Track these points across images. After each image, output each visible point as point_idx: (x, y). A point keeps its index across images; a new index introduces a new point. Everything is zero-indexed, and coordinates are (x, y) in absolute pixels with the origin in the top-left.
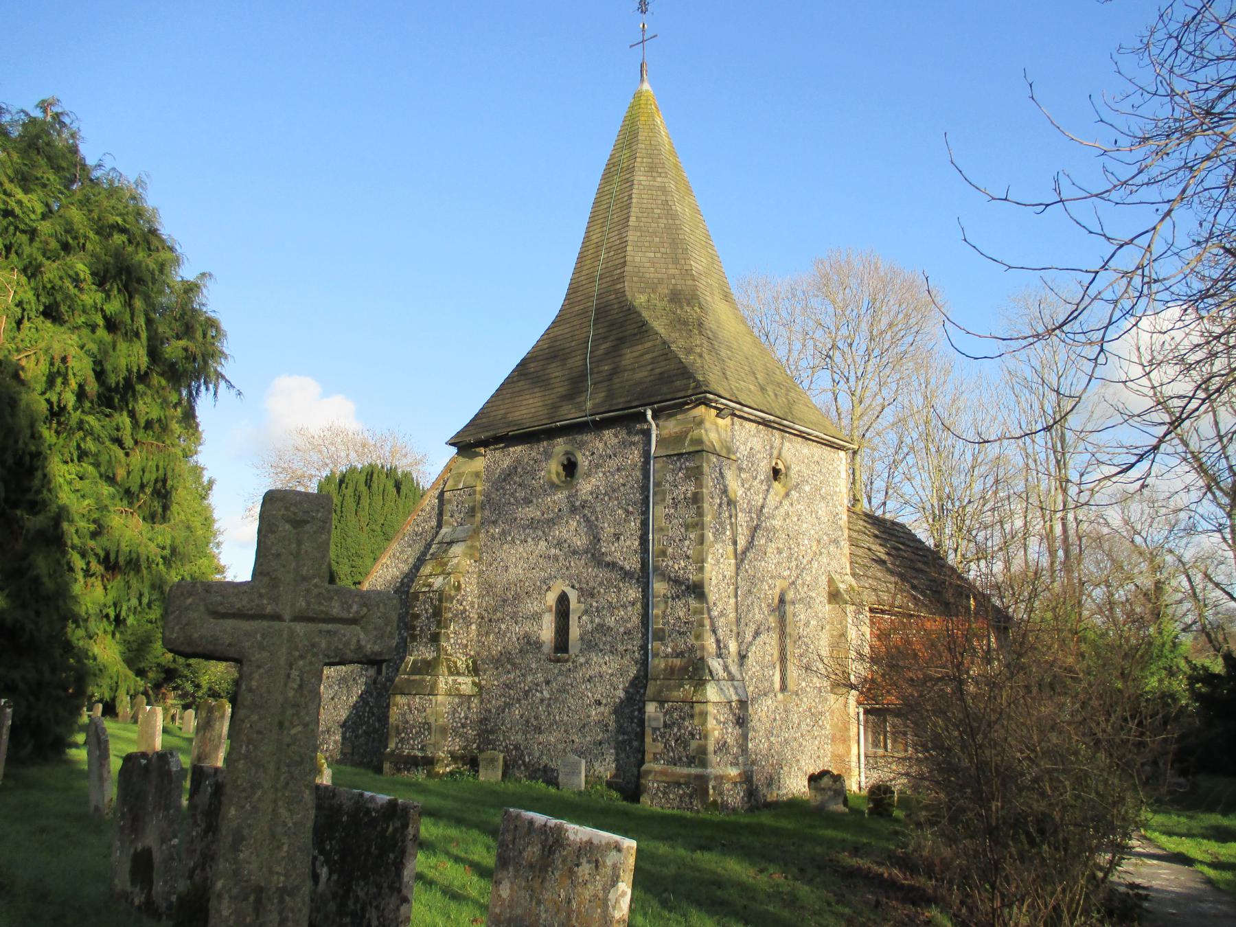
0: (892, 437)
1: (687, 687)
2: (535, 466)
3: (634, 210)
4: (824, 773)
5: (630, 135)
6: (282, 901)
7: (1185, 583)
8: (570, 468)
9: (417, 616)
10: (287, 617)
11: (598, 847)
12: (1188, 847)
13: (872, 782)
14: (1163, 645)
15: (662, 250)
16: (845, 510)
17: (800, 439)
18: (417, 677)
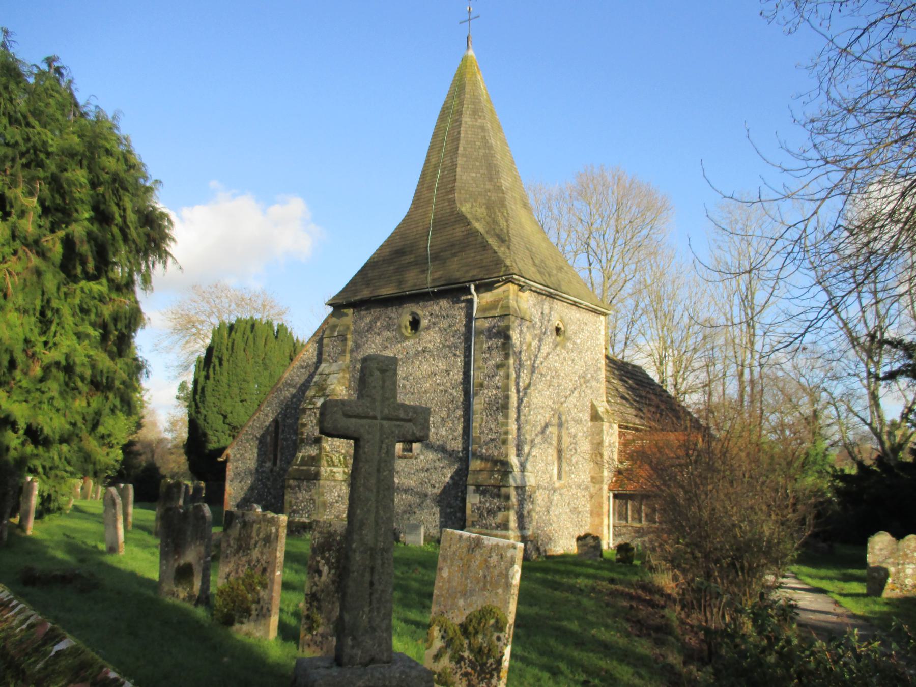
0: (630, 302)
1: (496, 476)
2: (390, 322)
3: (462, 143)
4: (587, 536)
5: (459, 88)
6: (382, 554)
7: (834, 412)
8: (415, 324)
9: (304, 425)
10: (379, 417)
11: (502, 547)
12: (824, 584)
13: (617, 543)
14: (817, 454)
15: (481, 171)
16: (603, 357)
17: (574, 307)
18: (305, 468)
